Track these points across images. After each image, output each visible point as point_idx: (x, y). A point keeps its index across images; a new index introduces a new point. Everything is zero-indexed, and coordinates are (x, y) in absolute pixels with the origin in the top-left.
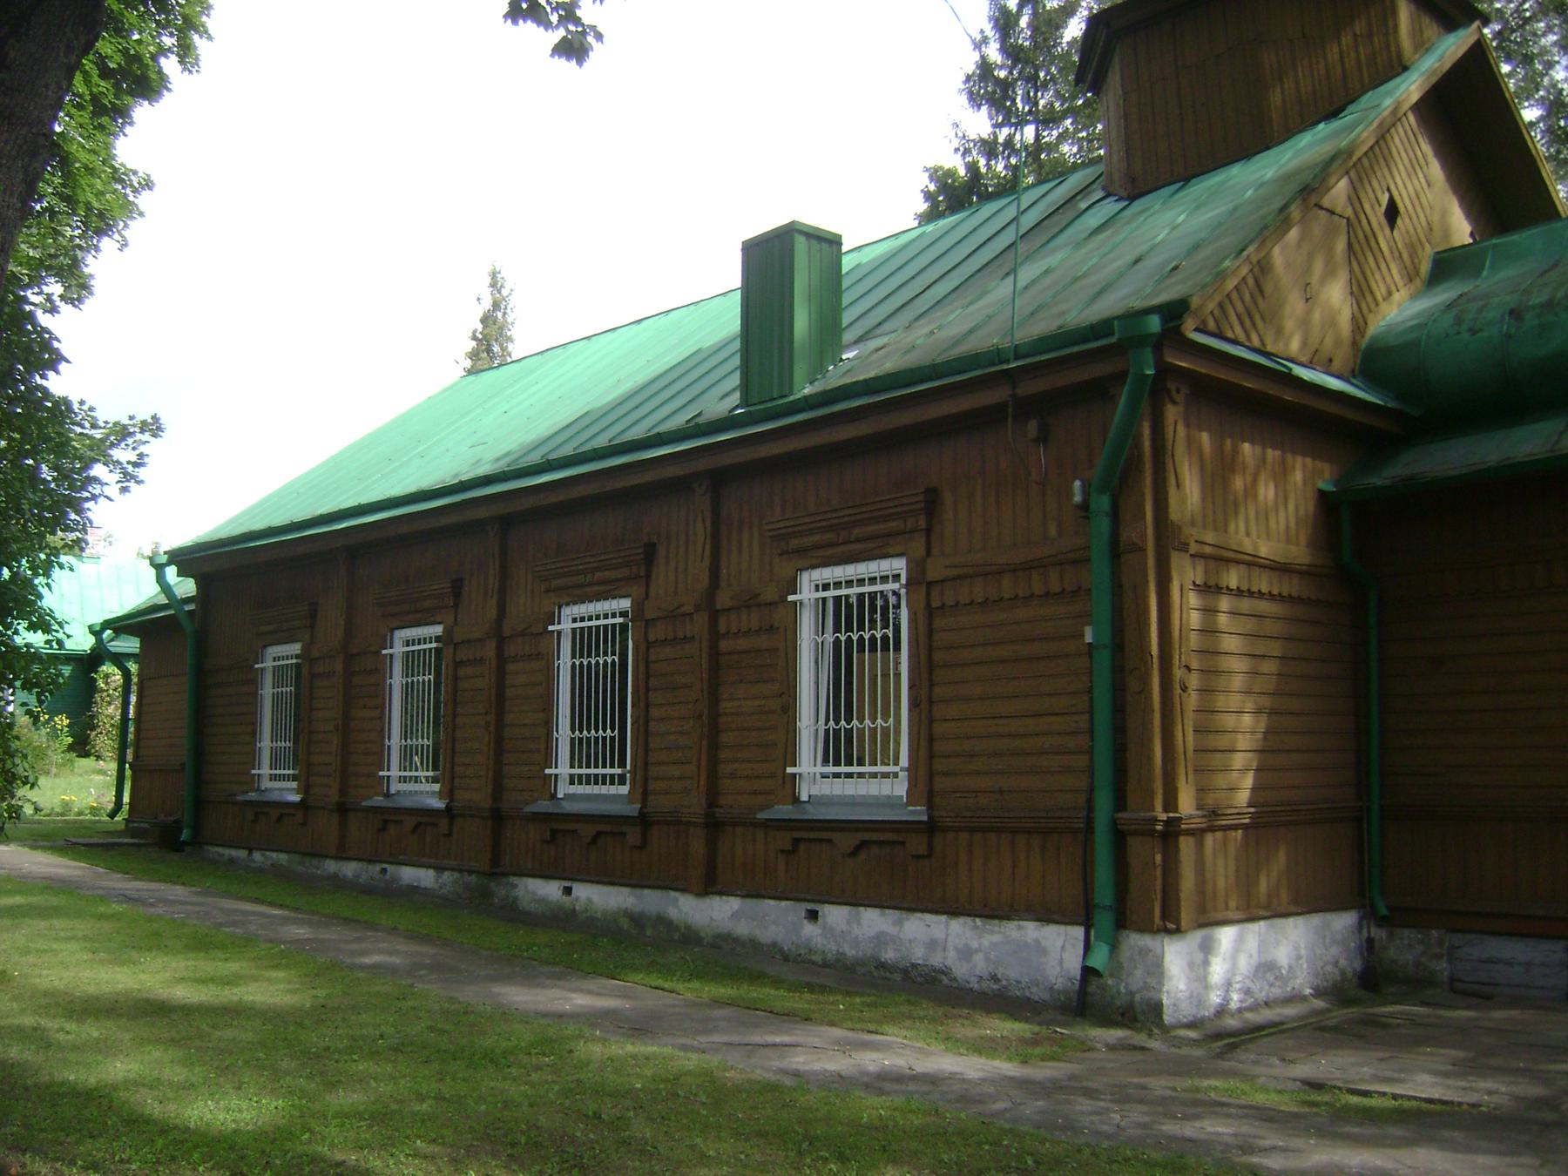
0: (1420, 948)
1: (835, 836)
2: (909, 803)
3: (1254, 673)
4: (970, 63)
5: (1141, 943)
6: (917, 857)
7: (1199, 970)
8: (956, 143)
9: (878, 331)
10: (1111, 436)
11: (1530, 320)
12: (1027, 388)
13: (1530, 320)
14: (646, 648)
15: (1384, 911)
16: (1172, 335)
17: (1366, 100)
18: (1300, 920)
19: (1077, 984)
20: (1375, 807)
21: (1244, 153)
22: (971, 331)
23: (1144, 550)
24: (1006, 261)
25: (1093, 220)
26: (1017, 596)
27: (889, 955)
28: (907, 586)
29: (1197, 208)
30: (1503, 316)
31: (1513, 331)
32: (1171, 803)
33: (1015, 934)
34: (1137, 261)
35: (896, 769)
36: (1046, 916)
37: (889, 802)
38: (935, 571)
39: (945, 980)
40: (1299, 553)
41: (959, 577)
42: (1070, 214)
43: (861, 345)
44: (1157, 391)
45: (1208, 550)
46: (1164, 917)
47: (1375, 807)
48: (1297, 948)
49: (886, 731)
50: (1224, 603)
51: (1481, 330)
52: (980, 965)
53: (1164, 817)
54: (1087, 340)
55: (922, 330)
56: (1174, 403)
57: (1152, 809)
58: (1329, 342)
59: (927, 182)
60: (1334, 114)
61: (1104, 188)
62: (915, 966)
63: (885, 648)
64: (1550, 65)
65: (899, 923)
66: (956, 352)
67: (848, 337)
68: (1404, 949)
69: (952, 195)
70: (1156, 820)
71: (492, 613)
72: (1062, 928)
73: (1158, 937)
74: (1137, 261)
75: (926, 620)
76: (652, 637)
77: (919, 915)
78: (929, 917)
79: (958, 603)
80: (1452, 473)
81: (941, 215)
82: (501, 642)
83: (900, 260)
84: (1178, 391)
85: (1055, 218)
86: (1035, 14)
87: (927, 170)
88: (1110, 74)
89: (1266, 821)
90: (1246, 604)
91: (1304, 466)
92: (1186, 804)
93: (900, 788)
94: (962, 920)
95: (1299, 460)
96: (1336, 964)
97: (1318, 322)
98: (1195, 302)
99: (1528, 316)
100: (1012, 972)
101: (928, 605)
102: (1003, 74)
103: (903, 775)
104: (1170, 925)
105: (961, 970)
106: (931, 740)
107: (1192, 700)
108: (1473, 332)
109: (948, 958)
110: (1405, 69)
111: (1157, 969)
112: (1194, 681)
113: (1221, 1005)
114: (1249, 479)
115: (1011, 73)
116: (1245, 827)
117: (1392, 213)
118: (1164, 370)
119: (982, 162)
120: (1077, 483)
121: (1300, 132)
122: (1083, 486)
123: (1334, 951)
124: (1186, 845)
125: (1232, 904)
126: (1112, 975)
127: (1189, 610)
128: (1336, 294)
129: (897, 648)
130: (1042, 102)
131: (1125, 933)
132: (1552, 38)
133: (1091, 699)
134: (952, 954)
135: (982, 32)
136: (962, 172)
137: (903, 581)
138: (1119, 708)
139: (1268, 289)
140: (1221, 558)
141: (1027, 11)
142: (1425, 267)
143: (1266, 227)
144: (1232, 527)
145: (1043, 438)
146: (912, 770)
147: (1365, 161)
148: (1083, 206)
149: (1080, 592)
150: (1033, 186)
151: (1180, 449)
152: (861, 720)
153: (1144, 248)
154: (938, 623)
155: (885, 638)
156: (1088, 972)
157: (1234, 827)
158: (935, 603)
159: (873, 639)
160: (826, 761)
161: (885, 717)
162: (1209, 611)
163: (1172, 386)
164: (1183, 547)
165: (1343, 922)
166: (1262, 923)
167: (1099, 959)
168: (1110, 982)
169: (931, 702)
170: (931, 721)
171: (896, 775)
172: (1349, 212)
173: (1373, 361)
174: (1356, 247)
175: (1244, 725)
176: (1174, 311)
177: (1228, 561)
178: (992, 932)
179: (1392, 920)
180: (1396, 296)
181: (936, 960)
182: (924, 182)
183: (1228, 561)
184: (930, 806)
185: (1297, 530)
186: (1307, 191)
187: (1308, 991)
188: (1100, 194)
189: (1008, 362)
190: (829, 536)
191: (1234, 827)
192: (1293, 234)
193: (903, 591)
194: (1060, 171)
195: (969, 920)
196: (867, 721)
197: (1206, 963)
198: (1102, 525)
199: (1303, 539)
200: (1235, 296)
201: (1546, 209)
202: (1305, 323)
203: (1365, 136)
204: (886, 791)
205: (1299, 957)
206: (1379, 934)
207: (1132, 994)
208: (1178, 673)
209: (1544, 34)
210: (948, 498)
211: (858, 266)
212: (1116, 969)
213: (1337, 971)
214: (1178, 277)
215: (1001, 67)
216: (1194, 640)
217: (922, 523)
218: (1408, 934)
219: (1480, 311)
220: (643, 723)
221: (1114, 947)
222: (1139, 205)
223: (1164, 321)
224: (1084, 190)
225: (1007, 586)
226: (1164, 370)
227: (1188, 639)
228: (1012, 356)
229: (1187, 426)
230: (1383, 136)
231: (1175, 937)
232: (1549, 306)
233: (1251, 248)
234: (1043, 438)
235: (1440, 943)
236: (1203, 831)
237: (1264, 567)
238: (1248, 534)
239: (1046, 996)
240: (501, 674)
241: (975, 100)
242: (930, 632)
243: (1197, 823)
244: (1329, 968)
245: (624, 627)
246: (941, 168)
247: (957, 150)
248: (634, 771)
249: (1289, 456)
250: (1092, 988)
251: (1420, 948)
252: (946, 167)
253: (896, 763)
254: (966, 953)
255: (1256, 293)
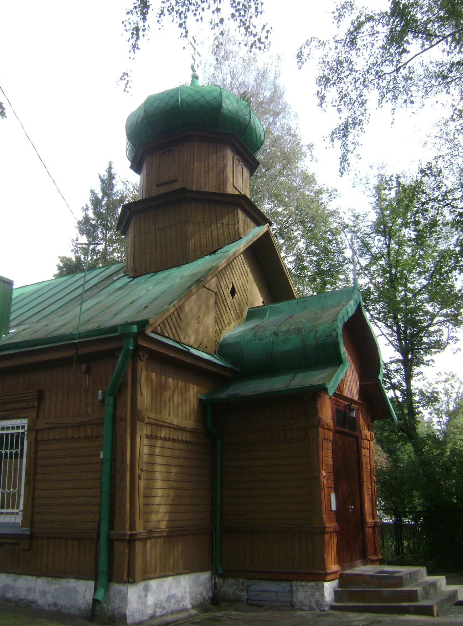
0: (235, 586)
2: (22, 527)
3: (169, 472)
4: (80, 217)
5: (118, 588)
6: (24, 550)
7: (143, 599)
8: (72, 248)
9: (26, 322)
10: (115, 371)
11: (281, 337)
12: (83, 351)
13: (281, 337)
15: (221, 571)
16: (141, 333)
17: (225, 248)
18: (187, 576)
19: (91, 606)
20: (218, 528)
21: (178, 264)
22: (63, 325)
23: (125, 420)
24: (81, 299)
25: (118, 284)
26: (73, 438)
27: (10, 595)
28: (28, 431)
29: (158, 284)
30: (271, 335)
31: (275, 340)
32: (132, 526)
33: (65, 585)
34: (132, 303)
35: (18, 511)
36: (79, 576)
37: (14, 525)
38: (40, 424)
39: (34, 606)
40: (189, 423)
41: (50, 428)
42: (110, 282)
43: (18, 327)
44: (136, 354)
45: (152, 421)
46: (129, 576)
47: (218, 528)
48: (185, 588)
50: (159, 443)
51: (263, 339)
52: (50, 599)
53: (129, 533)
54: (107, 333)
55: (44, 323)
56: (142, 361)
57: (125, 530)
58: (206, 340)
59: (60, 262)
60: (214, 252)
61: (124, 272)
62: (21, 600)
63: (16, 457)
64: (298, 241)
65: (15, 580)
66: (55, 334)
67: (12, 324)
68: (229, 587)
69: (69, 268)
70: (126, 535)
72: (85, 582)
73: (126, 585)
74: (132, 303)
75: (35, 445)
77: (24, 576)
78: (28, 577)
79: (42, 440)
80: (250, 394)
81: (64, 276)
83: (41, 294)
84: (143, 356)
85: (103, 282)
86: (109, 200)
87: (60, 258)
88: (129, 230)
89: (173, 534)
90: (167, 444)
91: (194, 388)
92: (140, 528)
93: (19, 519)
94: (43, 578)
95: (192, 386)
96: (201, 594)
97: (205, 332)
98: (151, 321)
99: (280, 335)
100: (63, 602)
101: (36, 440)
102: (94, 222)
103: (21, 513)
104: (131, 580)
105: (41, 601)
106: (34, 498)
107: (142, 484)
108: (260, 340)
109: (36, 596)
110: (241, 238)
111: (124, 599)
112: (144, 475)
113: (152, 614)
114: (171, 393)
115: (97, 222)
116: (165, 537)
117: (233, 292)
118: (138, 347)
119: (82, 257)
120: (100, 391)
121: (200, 258)
122: (103, 393)
123: (201, 589)
124: (138, 545)
125: (158, 570)
126: (106, 602)
127: (143, 448)
128: (209, 320)
129: (22, 457)
130: (108, 235)
131: (112, 583)
132: (298, 232)
133: (101, 483)
134: (37, 594)
135: (86, 205)
136: (74, 260)
137: (26, 429)
138: (112, 486)
139: (182, 316)
140: (158, 425)
141: (106, 199)
142: (245, 313)
143: (182, 294)
144: (163, 412)
145: (88, 371)
146: (25, 511)
147: (224, 271)
148: (115, 278)
149: (99, 437)
150: (102, 267)
151: (143, 379)
153: (135, 298)
154: (40, 447)
155: (16, 453)
156: (96, 601)
157: (160, 537)
158: (39, 439)
159: (11, 453)
161: (14, 489)
162: (152, 446)
163: (141, 354)
164: (142, 420)
165: (205, 576)
166: (170, 578)
167: (100, 595)
168: (105, 605)
169: (35, 482)
170: (34, 490)
171: (17, 513)
172: (216, 290)
173: (223, 349)
174: (219, 304)
175: (161, 493)
176: (143, 324)
177: (161, 426)
178: (55, 584)
179: (223, 576)
180: (233, 323)
181: (30, 597)
182: (58, 262)
183: (161, 426)
184: (32, 527)
185: (190, 415)
186: (200, 282)
187: (189, 606)
188: (123, 274)
189: (75, 339)
191: (160, 537)
192: (194, 297)
193: (26, 433)
194: (113, 262)
195: (45, 578)
197: (146, 596)
198: (109, 410)
199: (192, 418)
200: (169, 319)
201: (290, 295)
202: (197, 331)
203: (223, 263)
205: (186, 592)
206: (219, 581)
207: (114, 610)
208: (137, 472)
209: (296, 231)
210: (47, 395)
211: (23, 294)
212: (107, 599)
213: (201, 597)
214: (147, 311)
215: (93, 220)
216: (145, 458)
217: (36, 404)
218: (231, 581)
219: (263, 332)
221: (107, 590)
222: (136, 280)
223: (139, 328)
224: (117, 272)
225: (70, 433)
226: (138, 347)
227: (142, 458)
228: (77, 337)
229: (147, 370)
230: (229, 264)
231: (133, 585)
232: (288, 331)
233: (175, 302)
234: (88, 371)
235: (243, 584)
236: (146, 539)
237: (174, 428)
238: (169, 415)
239: (77, 612)
241: (82, 231)
242: (36, 451)
243: (143, 536)
244: (198, 596)
246: (65, 257)
247: (72, 250)
249: (188, 384)
250: (97, 608)
251: (235, 586)
252: (68, 257)
253: (18, 508)
254: (44, 594)
255: (178, 319)
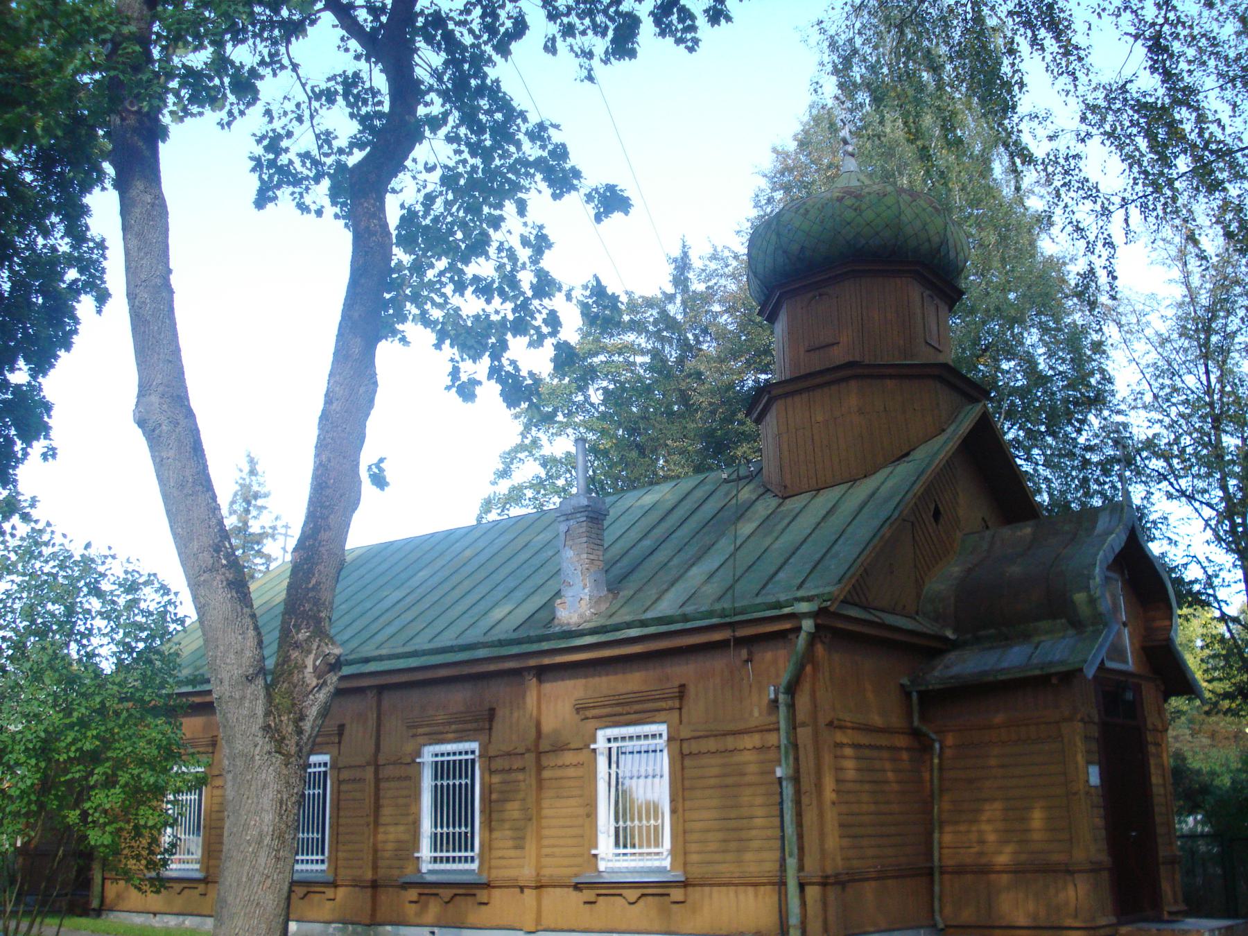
1: (440, 891)
14: (339, 782)
28: (480, 756)
37: (661, 870)
49: (656, 828)
71: (372, 749)
76: (341, 778)
82: (377, 767)
93: (667, 863)
146: (673, 852)
152: (640, 820)
160: (617, 844)
161: (656, 819)
190: (619, 709)
196: (644, 822)
204: (657, 864)
217: (487, 726)
220: (336, 826)
240: (377, 789)
245: (325, 773)
248: (330, 858)
